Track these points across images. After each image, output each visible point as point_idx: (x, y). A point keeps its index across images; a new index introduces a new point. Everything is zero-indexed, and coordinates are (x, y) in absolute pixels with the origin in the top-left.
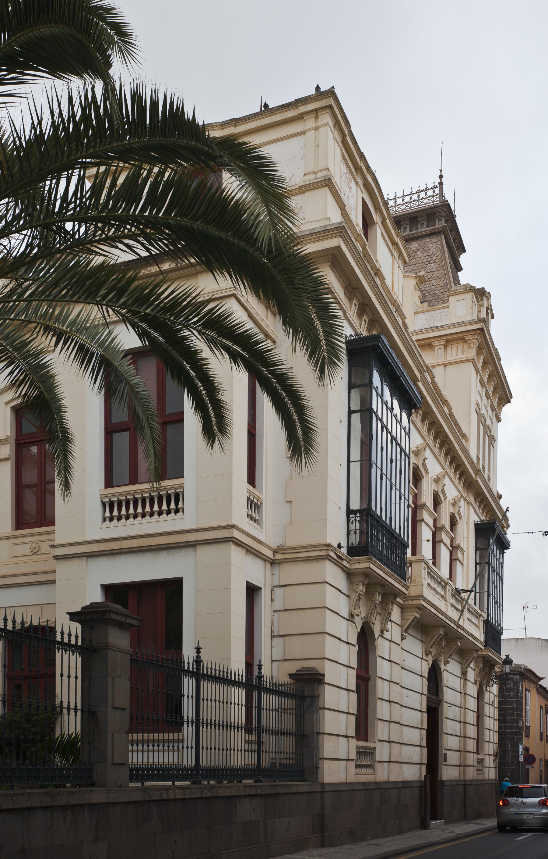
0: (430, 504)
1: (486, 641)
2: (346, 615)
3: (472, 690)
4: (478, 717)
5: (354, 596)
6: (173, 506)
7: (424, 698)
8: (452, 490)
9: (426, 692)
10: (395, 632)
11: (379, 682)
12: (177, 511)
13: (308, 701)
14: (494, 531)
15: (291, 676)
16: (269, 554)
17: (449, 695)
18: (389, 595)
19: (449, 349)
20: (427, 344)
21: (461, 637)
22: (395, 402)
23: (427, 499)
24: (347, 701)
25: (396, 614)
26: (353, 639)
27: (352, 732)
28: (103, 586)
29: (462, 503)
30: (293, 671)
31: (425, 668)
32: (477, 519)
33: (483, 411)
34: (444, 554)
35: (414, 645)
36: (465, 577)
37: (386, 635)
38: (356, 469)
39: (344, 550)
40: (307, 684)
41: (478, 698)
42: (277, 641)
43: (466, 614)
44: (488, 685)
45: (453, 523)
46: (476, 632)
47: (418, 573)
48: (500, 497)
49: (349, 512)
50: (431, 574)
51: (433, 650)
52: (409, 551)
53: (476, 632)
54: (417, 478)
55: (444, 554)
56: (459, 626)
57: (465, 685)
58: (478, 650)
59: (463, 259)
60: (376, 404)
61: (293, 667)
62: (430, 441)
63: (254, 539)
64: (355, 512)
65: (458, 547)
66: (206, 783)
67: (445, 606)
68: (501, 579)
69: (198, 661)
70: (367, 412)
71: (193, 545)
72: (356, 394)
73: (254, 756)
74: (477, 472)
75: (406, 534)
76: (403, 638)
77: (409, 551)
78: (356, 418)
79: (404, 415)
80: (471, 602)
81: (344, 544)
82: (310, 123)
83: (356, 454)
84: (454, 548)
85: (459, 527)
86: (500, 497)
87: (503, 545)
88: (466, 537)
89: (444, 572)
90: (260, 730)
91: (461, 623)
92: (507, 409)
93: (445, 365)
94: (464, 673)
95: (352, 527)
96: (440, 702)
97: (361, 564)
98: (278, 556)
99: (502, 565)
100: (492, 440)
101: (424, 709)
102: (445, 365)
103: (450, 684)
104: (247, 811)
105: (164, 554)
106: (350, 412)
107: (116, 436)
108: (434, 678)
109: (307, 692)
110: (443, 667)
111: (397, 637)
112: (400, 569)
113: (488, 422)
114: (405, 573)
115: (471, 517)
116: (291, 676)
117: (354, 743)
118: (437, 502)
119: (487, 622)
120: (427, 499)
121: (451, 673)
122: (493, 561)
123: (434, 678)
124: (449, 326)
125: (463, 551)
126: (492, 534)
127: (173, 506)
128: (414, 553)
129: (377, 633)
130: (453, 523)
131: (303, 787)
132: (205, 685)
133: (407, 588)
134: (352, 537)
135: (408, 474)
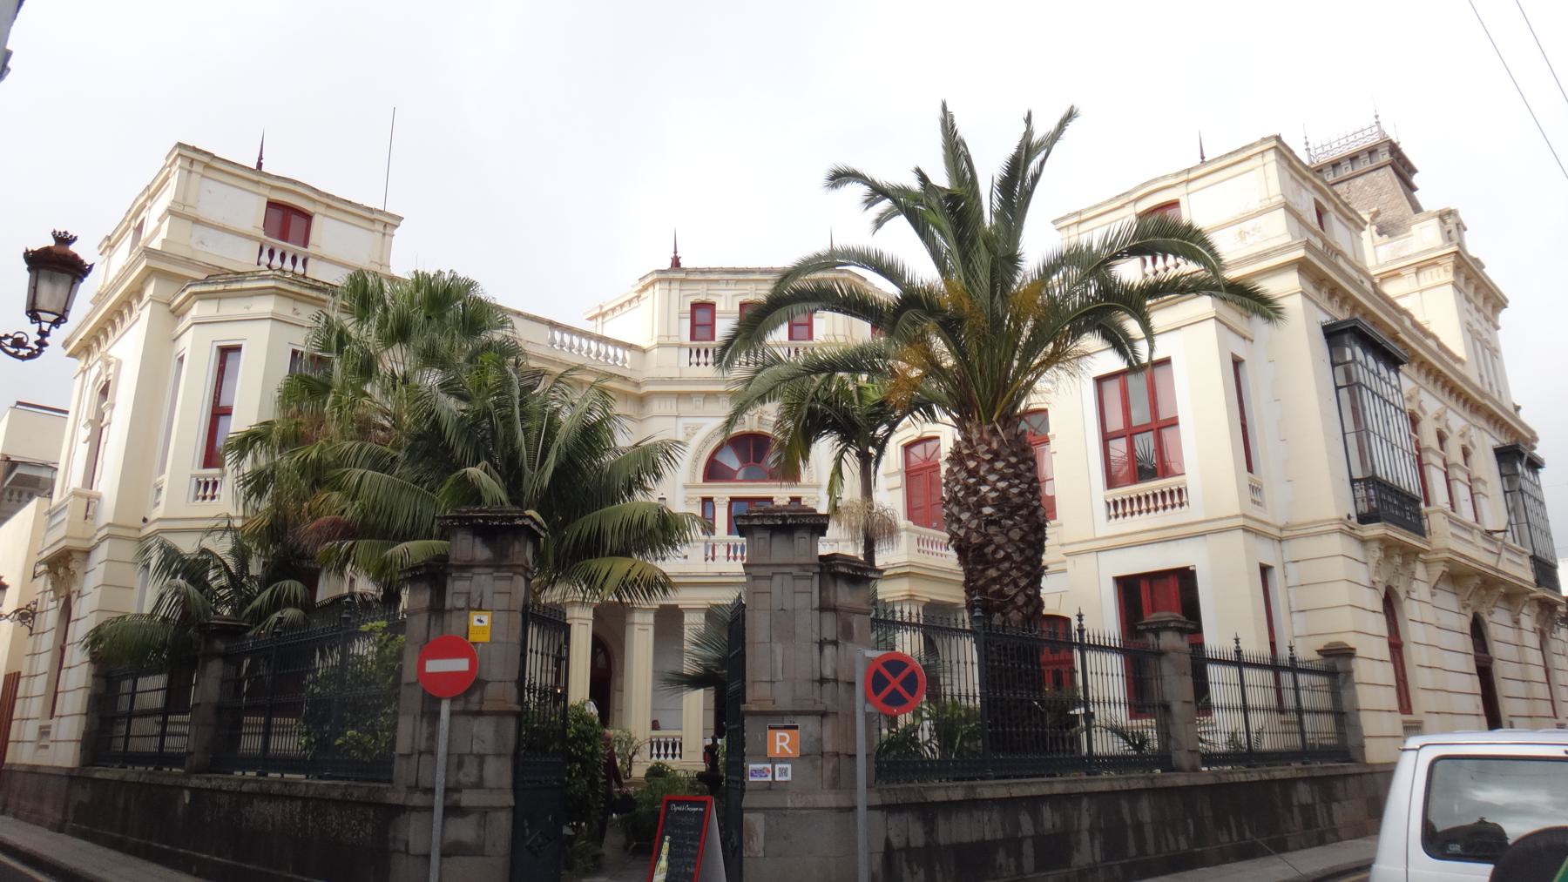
0: (1435, 444)
1: (1537, 581)
2: (1367, 583)
3: (1532, 640)
4: (1547, 672)
5: (1372, 563)
6: (1176, 500)
7: (1471, 658)
8: (1457, 421)
9: (1471, 650)
10: (1421, 590)
11: (1414, 647)
12: (1181, 505)
13: (1341, 676)
14: (1521, 455)
15: (1319, 652)
16: (1276, 532)
17: (1498, 650)
18: (1410, 555)
19: (1421, 276)
20: (1395, 275)
21: (1503, 582)
22: (1382, 367)
23: (1430, 440)
24: (1386, 673)
25: (1420, 570)
26: (1380, 607)
27: (1395, 705)
28: (1120, 581)
29: (1473, 431)
30: (1321, 647)
31: (1465, 623)
32: (1496, 444)
33: (1477, 326)
34: (1462, 492)
35: (1448, 600)
36: (1494, 513)
37: (1414, 595)
38: (1352, 439)
39: (1354, 520)
40: (1336, 662)
41: (1542, 649)
42: (1296, 617)
43: (1505, 555)
44: (1551, 630)
45: (1466, 453)
46: (1523, 572)
47: (1437, 522)
48: (1517, 408)
49: (1353, 481)
50: (1454, 522)
51: (1472, 602)
52: (1422, 505)
53: (1523, 572)
54: (1414, 421)
55: (1462, 492)
56: (1498, 571)
57: (1520, 636)
58: (1528, 592)
59: (1416, 180)
60: (1361, 375)
61: (1321, 643)
62: (1422, 381)
63: (1262, 522)
64: (1359, 481)
65: (1478, 479)
66: (782, 742)
67: (1478, 553)
68: (1542, 503)
69: (1292, 659)
70: (1353, 386)
71: (1202, 534)
72: (1340, 370)
73: (1298, 737)
74: (1482, 394)
75: (1415, 489)
76: (1433, 595)
77: (1422, 505)
78: (1344, 393)
79: (1392, 374)
80: (1509, 540)
81: (1353, 514)
82: (1257, 161)
83: (1349, 426)
84: (1472, 481)
85: (1473, 458)
86: (1517, 408)
87: (1535, 465)
88: (1486, 466)
89: (1466, 514)
90: (1300, 711)
91: (1500, 567)
92: (1504, 317)
93: (1421, 291)
94: (1517, 622)
95: (1358, 495)
96: (1491, 660)
97: (1375, 530)
98: (1285, 534)
99: (1539, 487)
100: (1495, 352)
101: (1474, 671)
102: (1421, 291)
103: (1500, 637)
104: (1303, 794)
105: (1173, 544)
106: (1337, 388)
107: (1112, 443)
108: (1478, 631)
109: (1339, 667)
110: (1487, 618)
111: (1427, 597)
112: (1418, 528)
113: (1486, 336)
114: (1422, 527)
115: (1486, 442)
116: (1319, 652)
117: (1399, 717)
118: (1441, 438)
119: (1534, 558)
120: (1430, 440)
121: (1499, 625)
122: (1526, 486)
123: (1478, 631)
124: (1417, 255)
125: (1484, 483)
126: (1516, 455)
127: (1176, 500)
128: (1428, 504)
129: (1402, 595)
130: (1466, 453)
131: (1352, 768)
132: (1247, 672)
133: (1429, 543)
134: (1360, 504)
135: (1405, 425)
